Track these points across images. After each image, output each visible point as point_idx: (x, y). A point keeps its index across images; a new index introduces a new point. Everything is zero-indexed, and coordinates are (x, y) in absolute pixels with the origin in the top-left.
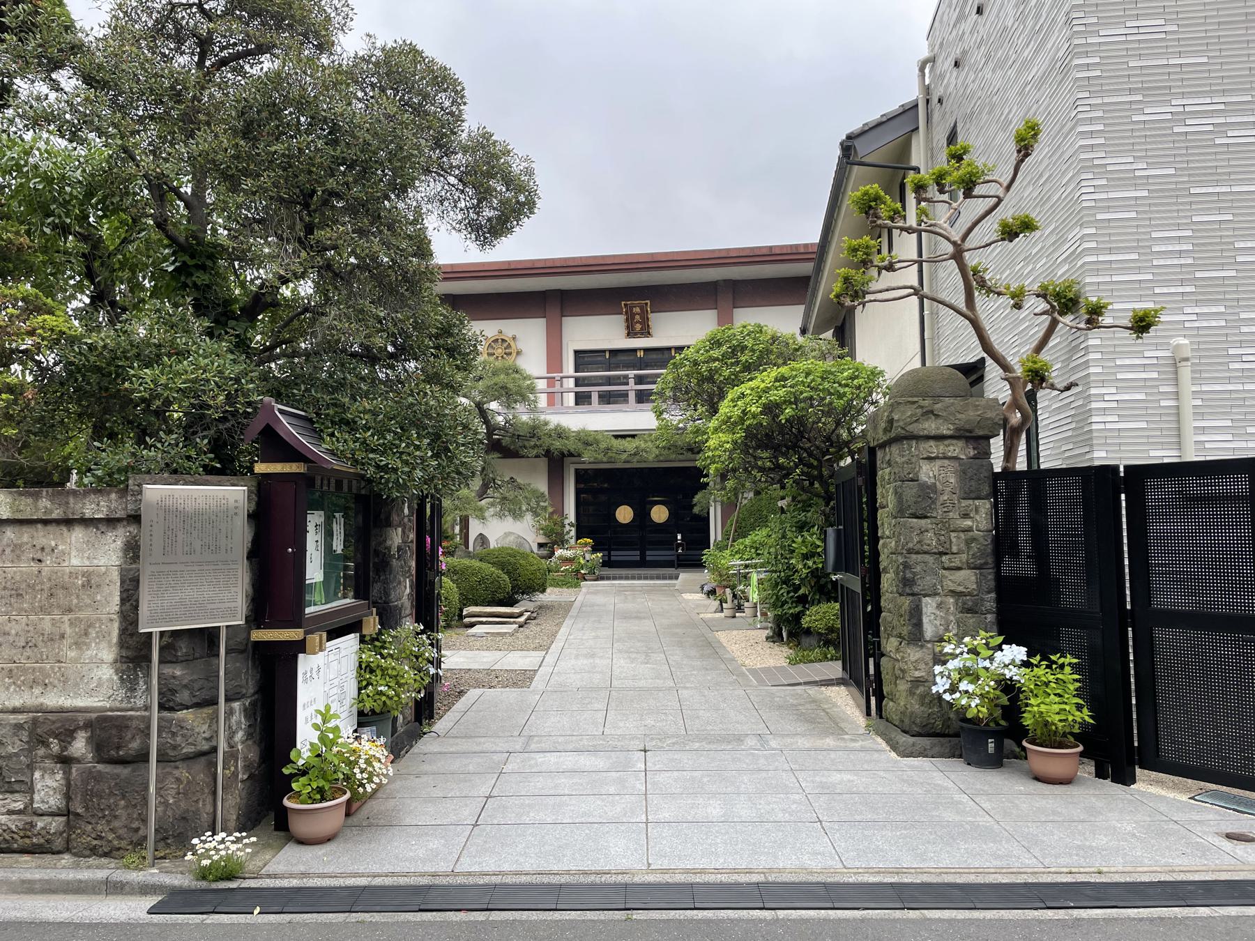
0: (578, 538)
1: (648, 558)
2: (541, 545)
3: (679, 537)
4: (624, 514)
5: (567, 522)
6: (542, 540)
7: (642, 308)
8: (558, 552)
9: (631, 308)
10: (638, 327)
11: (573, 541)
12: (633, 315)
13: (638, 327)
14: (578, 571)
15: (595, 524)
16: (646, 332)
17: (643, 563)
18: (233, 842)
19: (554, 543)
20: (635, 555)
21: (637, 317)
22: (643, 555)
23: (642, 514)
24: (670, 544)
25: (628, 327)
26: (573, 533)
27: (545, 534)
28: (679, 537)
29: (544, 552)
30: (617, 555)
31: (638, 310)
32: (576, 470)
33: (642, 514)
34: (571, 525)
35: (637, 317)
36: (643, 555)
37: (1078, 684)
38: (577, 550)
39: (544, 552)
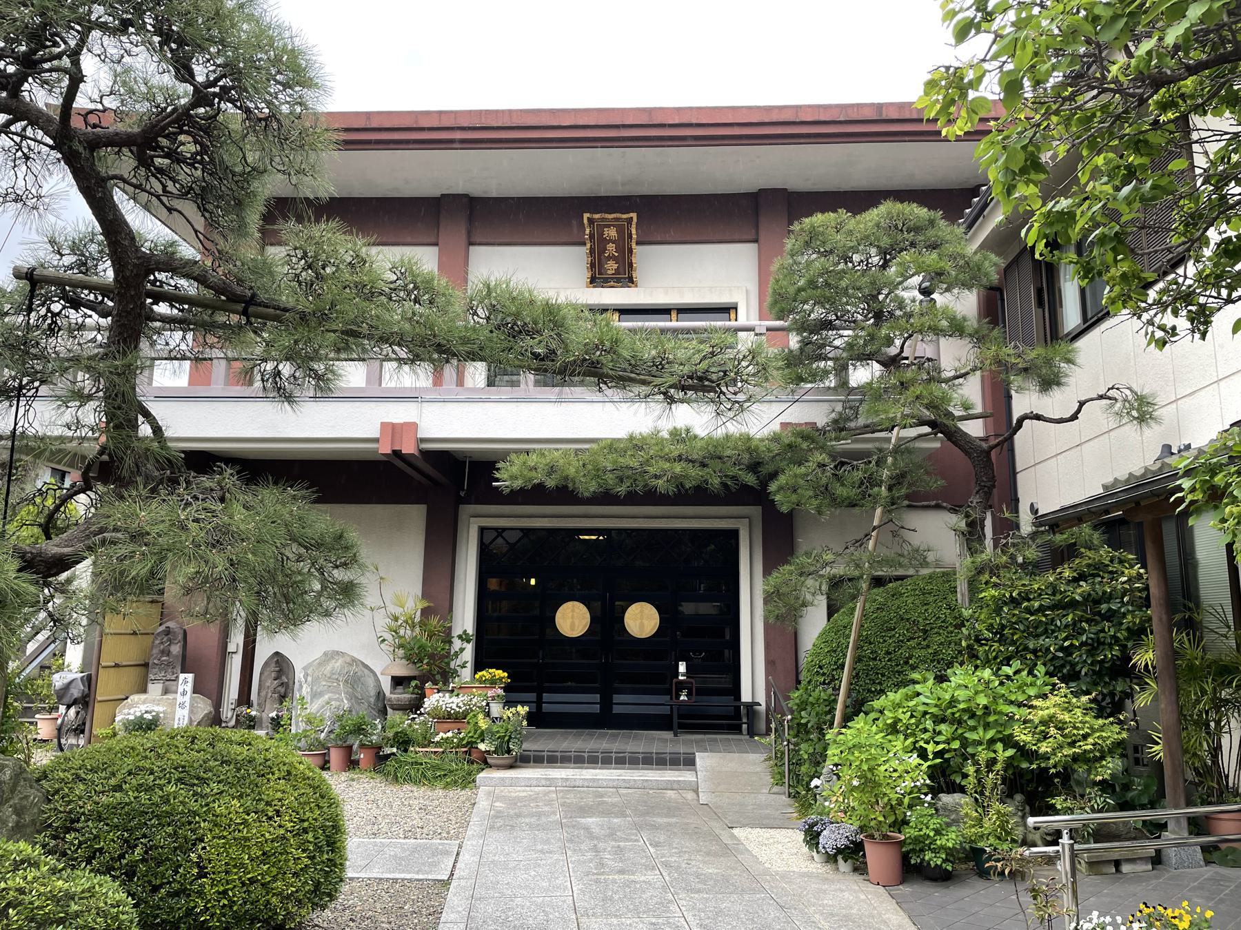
0: (478, 667)
1: (617, 710)
2: (398, 681)
3: (682, 668)
4: (573, 619)
5: (457, 631)
6: (402, 670)
7: (620, 230)
8: (434, 700)
9: (601, 228)
10: (611, 267)
11: (466, 674)
12: (603, 242)
13: (611, 267)
14: (471, 745)
15: (513, 640)
16: (626, 278)
17: (605, 720)
18: (913, 382)
19: (423, 679)
20: (589, 702)
21: (611, 247)
22: (606, 703)
23: (607, 621)
24: (664, 682)
25: (592, 265)
26: (468, 654)
27: (408, 658)
28: (682, 668)
29: (404, 696)
30: (555, 702)
31: (612, 233)
32: (482, 530)
33: (607, 621)
34: (464, 637)
35: (611, 247)
36: (606, 703)
37: (498, 475)
38: (474, 695)
39: (404, 696)
